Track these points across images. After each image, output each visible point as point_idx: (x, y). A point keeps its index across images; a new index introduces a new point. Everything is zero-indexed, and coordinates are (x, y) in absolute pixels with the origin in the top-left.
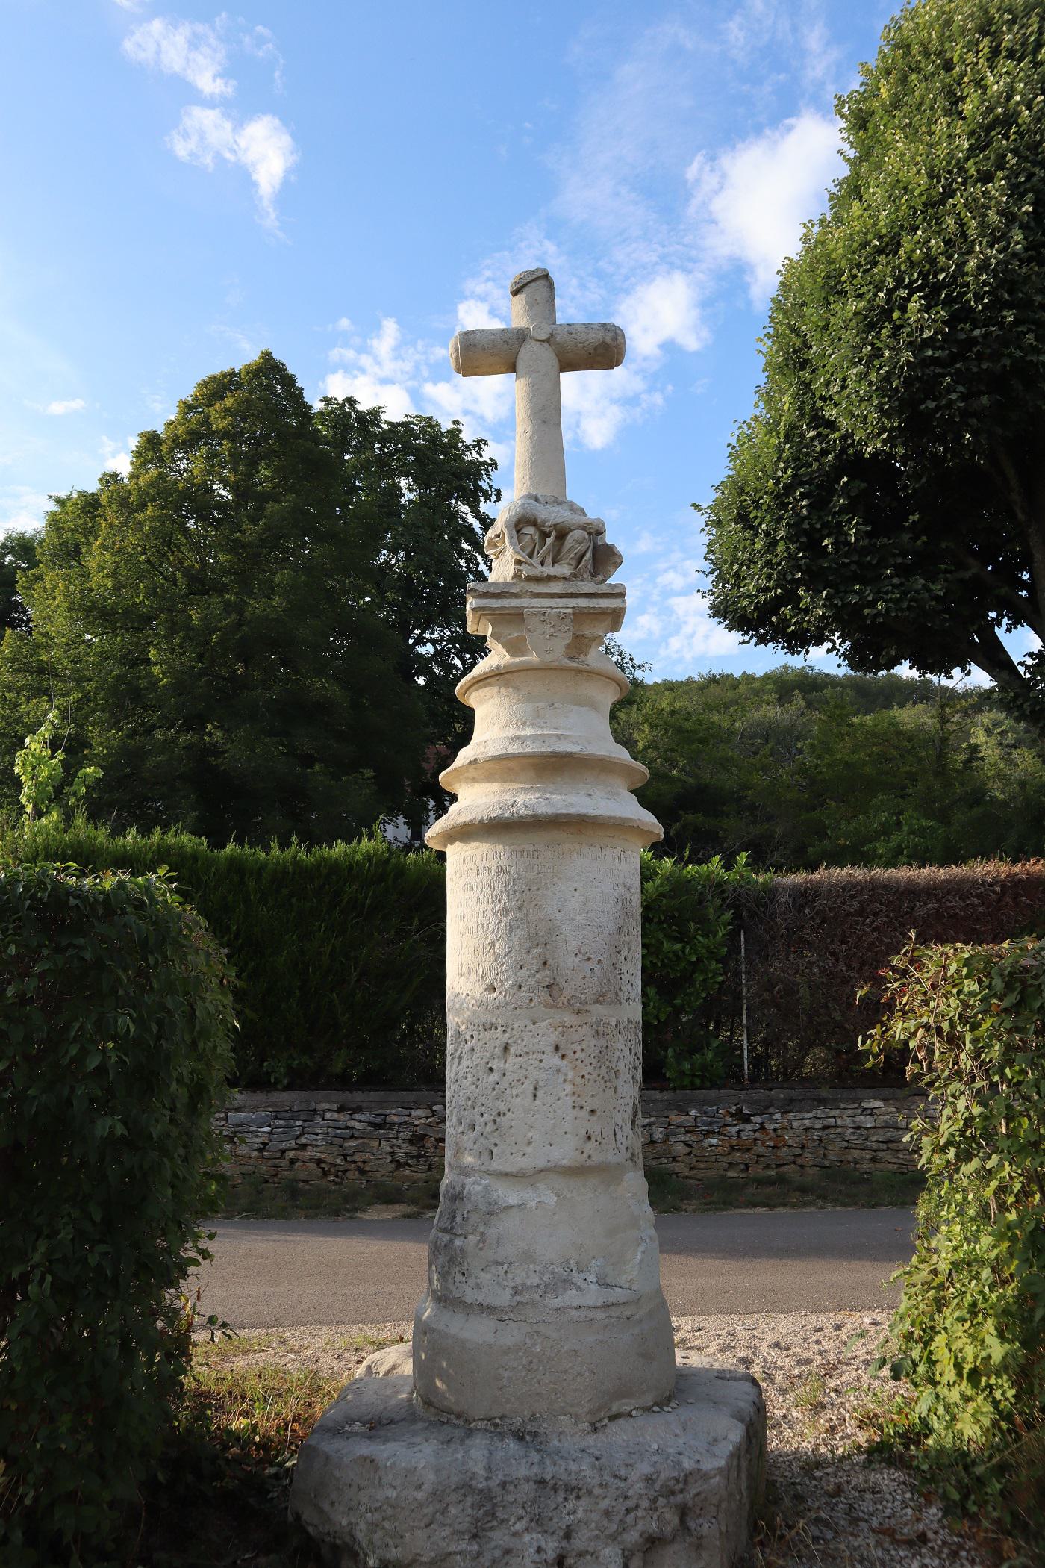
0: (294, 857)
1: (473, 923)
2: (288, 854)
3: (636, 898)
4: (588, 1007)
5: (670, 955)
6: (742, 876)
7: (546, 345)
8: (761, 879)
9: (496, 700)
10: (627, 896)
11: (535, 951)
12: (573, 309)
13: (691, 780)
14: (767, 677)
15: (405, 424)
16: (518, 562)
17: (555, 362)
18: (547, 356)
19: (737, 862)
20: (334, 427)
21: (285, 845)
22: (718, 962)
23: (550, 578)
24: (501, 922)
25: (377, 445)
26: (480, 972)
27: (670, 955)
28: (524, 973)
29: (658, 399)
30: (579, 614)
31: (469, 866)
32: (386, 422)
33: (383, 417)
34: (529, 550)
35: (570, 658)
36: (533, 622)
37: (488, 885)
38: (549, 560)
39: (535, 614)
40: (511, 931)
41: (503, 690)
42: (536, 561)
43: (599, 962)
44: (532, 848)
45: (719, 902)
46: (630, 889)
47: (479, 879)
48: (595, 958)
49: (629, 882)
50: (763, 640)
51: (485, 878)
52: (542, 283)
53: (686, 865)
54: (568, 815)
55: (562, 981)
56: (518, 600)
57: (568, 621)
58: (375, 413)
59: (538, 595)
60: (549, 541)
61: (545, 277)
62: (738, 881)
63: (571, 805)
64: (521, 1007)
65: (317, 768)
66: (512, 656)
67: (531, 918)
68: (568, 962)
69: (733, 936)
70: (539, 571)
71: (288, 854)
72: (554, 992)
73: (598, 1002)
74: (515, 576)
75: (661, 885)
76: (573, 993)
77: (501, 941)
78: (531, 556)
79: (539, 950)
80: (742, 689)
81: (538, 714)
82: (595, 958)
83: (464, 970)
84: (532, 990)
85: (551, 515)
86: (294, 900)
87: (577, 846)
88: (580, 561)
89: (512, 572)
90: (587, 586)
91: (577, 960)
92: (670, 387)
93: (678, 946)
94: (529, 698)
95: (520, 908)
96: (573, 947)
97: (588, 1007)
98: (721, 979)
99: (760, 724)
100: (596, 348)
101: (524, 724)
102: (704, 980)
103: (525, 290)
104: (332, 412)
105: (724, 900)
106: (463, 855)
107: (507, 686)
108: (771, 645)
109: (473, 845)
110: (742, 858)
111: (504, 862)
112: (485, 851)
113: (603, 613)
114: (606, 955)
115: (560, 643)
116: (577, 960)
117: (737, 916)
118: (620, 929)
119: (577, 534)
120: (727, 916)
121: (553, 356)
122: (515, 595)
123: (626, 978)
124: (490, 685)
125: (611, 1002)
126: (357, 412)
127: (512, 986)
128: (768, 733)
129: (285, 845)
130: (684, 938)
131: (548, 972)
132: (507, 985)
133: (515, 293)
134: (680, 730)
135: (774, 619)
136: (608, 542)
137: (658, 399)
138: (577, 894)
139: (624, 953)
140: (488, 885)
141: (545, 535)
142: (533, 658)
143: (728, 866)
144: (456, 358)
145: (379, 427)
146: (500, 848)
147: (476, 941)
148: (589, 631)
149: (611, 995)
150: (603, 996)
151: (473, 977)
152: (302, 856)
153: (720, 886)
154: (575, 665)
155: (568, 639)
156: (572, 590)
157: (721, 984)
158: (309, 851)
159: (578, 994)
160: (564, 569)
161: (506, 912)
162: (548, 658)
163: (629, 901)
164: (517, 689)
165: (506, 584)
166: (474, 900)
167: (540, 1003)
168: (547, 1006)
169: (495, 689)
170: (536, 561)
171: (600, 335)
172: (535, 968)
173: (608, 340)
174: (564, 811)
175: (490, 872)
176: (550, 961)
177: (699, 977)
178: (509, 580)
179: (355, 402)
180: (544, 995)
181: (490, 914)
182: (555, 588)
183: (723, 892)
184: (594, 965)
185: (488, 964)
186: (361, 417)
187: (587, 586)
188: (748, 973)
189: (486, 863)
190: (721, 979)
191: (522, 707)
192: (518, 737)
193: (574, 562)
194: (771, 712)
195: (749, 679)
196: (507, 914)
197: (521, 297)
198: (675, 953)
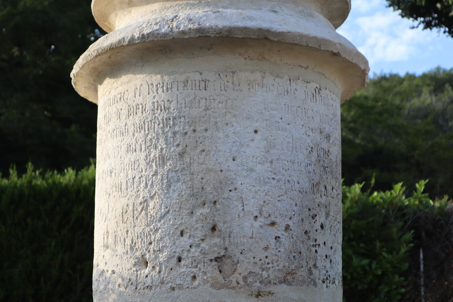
0: (30, 182)
1: (122, 178)
2: (25, 179)
3: (336, 152)
4: (271, 288)
5: (359, 269)
6: (421, 202)
8: (437, 204)
10: (325, 145)
11: (200, 212)
13: (370, 145)
14: (424, 76)
19: (416, 190)
21: (21, 171)
22: (400, 276)
24: (156, 173)
26: (128, 242)
27: (359, 269)
28: (185, 241)
31: (119, 106)
37: (141, 128)
40: (169, 186)
43: (287, 228)
44: (198, 77)
45: (401, 224)
46: (328, 137)
47: (130, 122)
48: (282, 223)
49: (327, 129)
50: (428, 25)
51: (137, 119)
53: (372, 193)
54: (245, 29)
55: (237, 252)
62: (418, 206)
63: (251, 18)
64: (180, 287)
65: (74, 127)
67: (195, 167)
68: (245, 227)
69: (413, 255)
71: (25, 179)
72: (227, 268)
73: (284, 281)
75: (351, 207)
76: (251, 268)
77: (156, 200)
79: (205, 210)
80: (406, 84)
82: (282, 223)
83: (111, 240)
84: (195, 263)
86: (29, 220)
87: (258, 76)
91: (257, 224)
93: (365, 262)
95: (182, 155)
96: (252, 207)
97: (271, 288)
98: (403, 290)
99: (419, 109)
102: (388, 292)
105: (405, 222)
106: (113, 93)
108: (435, 29)
109: (125, 78)
110: (421, 186)
111: (162, 96)
112: (138, 83)
114: (295, 219)
116: (257, 224)
117: (417, 237)
118: (315, 186)
120: (409, 236)
123: (322, 251)
125: (303, 282)
127: (169, 258)
128: (424, 113)
129: (21, 171)
130: (371, 255)
131: (217, 240)
132: (162, 257)
134: (361, 106)
135: (439, 6)
138: (258, 137)
139: (321, 219)
140: (141, 128)
143: (410, 191)
146: (156, 79)
147: (124, 201)
149: (302, 273)
150: (291, 273)
151: (120, 249)
152: (39, 182)
153: (401, 211)
157: (403, 295)
158: (42, 175)
159: (257, 270)
161: (163, 160)
163: (327, 153)
166: (124, 148)
167: (205, 282)
168: (216, 285)
172: (199, 234)
174: (241, 24)
175: (144, 110)
176: (220, 226)
177: (384, 289)
180: (212, 271)
181: (143, 165)
183: (404, 215)
184: (279, 231)
185: (138, 230)
188: (426, 286)
189: (139, 100)
190: (403, 290)
194: (427, 98)
195: (411, 77)
196: (164, 164)
198: (363, 268)
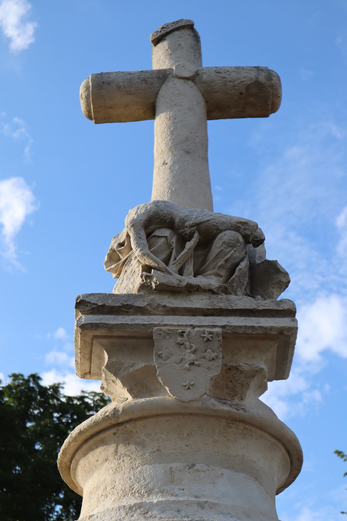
7: (190, 83)
9: (112, 464)
12: (221, 55)
15: (81, 398)
16: (147, 269)
17: (200, 109)
18: (192, 96)
20: (19, 399)
23: (191, 290)
25: (56, 415)
29: (317, 395)
30: (230, 337)
32: (65, 397)
33: (62, 391)
34: (164, 256)
35: (219, 399)
36: (166, 346)
38: (190, 268)
39: (169, 334)
41: (122, 449)
42: (173, 268)
52: (186, 33)
56: (145, 317)
57: (216, 344)
58: (56, 388)
59: (174, 311)
60: (189, 245)
61: (190, 27)
66: (135, 396)
70: (174, 279)
74: (142, 287)
78: (167, 261)
81: (171, 478)
85: (188, 211)
88: (232, 271)
89: (139, 281)
90: (242, 301)
92: (327, 387)
94: (159, 456)
100: (248, 87)
101: (150, 492)
103: (168, 38)
104: (18, 386)
107: (127, 441)
113: (266, 335)
115: (204, 378)
119: (228, 235)
121: (201, 99)
122: (142, 311)
124: (103, 442)
126: (40, 387)
133: (157, 41)
136: (270, 257)
137: (317, 395)
141: (183, 240)
142: (167, 396)
144: (87, 98)
145: (58, 400)
148: (248, 361)
154: (226, 408)
155: (216, 369)
156: (222, 305)
160: (210, 281)
162: (188, 396)
164: (142, 445)
165: (129, 296)
169: (111, 448)
170: (173, 268)
171: (253, 75)
173: (262, 78)
178: (135, 292)
179: (39, 378)
182: (198, 302)
186: (43, 391)
187: (242, 301)
191: (148, 470)
192: (140, 506)
193: (223, 273)
197: (164, 45)
